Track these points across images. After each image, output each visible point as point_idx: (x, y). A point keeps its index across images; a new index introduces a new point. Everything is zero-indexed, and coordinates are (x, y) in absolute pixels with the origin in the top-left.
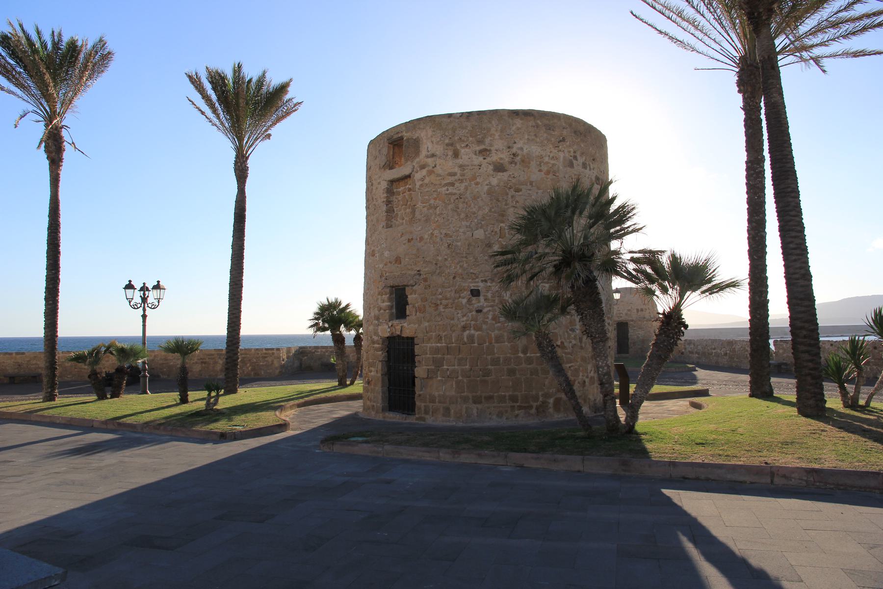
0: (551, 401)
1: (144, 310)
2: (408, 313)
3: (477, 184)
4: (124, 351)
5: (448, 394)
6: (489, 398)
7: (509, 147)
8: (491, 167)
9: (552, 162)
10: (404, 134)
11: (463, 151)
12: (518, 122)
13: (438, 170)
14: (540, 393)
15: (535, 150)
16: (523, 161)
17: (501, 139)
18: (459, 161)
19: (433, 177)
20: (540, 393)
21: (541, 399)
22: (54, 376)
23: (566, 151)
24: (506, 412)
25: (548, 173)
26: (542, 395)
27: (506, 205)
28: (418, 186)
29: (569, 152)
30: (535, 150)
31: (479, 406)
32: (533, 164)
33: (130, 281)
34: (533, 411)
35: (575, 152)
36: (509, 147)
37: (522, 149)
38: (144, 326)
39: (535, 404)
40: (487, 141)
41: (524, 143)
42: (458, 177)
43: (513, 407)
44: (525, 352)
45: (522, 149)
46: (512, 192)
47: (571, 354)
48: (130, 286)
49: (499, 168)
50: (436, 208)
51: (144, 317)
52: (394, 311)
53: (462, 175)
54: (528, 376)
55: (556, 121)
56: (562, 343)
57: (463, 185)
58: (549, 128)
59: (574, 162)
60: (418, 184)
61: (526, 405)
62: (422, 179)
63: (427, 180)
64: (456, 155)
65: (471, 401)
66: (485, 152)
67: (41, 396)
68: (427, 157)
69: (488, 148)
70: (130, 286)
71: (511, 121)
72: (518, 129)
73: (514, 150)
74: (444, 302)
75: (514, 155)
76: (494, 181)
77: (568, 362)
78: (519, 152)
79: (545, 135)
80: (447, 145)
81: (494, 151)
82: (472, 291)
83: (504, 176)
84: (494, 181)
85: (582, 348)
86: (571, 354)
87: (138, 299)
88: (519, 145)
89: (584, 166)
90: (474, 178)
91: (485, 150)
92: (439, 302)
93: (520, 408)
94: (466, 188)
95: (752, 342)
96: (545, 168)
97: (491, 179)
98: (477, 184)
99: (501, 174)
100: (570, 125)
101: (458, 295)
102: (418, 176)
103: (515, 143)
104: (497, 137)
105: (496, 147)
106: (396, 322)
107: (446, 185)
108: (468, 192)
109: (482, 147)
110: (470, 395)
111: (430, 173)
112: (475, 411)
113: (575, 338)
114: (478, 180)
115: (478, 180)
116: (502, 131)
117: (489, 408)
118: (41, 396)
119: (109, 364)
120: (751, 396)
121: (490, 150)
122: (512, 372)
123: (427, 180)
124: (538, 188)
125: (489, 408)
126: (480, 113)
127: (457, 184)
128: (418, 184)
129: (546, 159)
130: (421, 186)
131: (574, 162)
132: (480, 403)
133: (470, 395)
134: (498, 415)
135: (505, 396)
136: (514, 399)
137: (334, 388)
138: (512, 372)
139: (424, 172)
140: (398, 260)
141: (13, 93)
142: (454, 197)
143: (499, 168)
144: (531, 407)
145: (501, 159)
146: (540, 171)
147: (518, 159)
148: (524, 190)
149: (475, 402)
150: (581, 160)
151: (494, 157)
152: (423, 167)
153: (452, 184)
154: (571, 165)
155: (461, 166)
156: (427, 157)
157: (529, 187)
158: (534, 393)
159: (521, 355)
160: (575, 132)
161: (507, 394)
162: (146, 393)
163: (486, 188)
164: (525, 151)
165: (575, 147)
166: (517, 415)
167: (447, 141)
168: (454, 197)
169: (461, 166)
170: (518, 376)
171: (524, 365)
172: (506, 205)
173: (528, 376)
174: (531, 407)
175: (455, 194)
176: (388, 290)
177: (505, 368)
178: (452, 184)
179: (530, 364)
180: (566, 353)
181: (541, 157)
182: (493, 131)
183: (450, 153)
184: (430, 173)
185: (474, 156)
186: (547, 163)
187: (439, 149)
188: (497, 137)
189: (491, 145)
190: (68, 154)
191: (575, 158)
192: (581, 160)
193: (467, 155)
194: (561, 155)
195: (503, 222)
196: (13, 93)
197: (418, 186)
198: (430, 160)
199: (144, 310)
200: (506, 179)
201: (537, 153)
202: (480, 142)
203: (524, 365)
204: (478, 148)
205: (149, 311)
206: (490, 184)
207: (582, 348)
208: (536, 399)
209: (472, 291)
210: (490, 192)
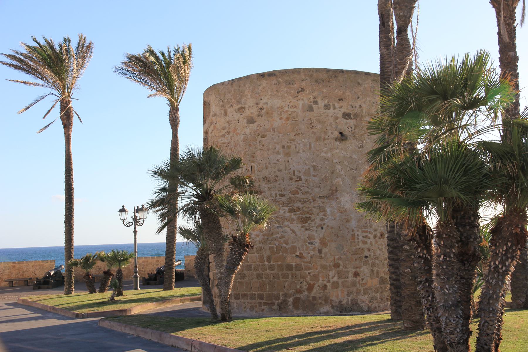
0: (291, 300)
1: (135, 228)
3: (237, 134)
4: (117, 257)
6: (245, 295)
8: (245, 121)
11: (229, 110)
14: (281, 293)
15: (277, 102)
16: (267, 113)
17: (252, 97)
18: (227, 118)
20: (281, 293)
21: (281, 298)
22: (71, 276)
23: (305, 99)
24: (256, 306)
25: (288, 119)
26: (283, 295)
27: (255, 148)
29: (309, 99)
30: (277, 102)
31: (238, 301)
32: (275, 114)
33: (123, 206)
34: (275, 307)
35: (315, 98)
36: (257, 104)
37: (266, 103)
38: (135, 239)
39: (277, 302)
40: (243, 101)
41: (268, 99)
42: (227, 130)
43: (260, 303)
44: (269, 260)
45: (266, 103)
46: (259, 138)
47: (310, 262)
48: (123, 210)
49: (251, 121)
51: (135, 232)
54: (271, 279)
55: (295, 76)
56: (300, 253)
57: (229, 136)
58: (289, 83)
59: (314, 106)
61: (270, 302)
64: (226, 114)
66: (241, 110)
67: (63, 293)
70: (123, 210)
71: (259, 83)
72: (264, 88)
73: (260, 106)
76: (248, 131)
77: (306, 269)
78: (265, 106)
79: (286, 89)
81: (247, 108)
83: (254, 126)
84: (248, 131)
85: (321, 258)
86: (310, 262)
87: (130, 219)
90: (235, 130)
91: (242, 108)
93: (265, 304)
95: (197, 263)
96: (285, 116)
99: (252, 125)
100: (311, 76)
103: (261, 99)
104: (249, 97)
105: (249, 104)
108: (232, 141)
109: (240, 106)
113: (314, 250)
114: (238, 131)
115: (238, 131)
116: (252, 92)
117: (244, 303)
118: (63, 293)
119: (101, 267)
120: (90, 293)
121: (244, 108)
122: (259, 276)
124: (280, 133)
125: (244, 303)
127: (227, 136)
129: (286, 108)
131: (314, 106)
132: (239, 299)
134: (250, 309)
135: (255, 294)
136: (261, 297)
138: (259, 276)
141: (36, 84)
142: (225, 145)
143: (251, 121)
144: (273, 304)
145: (252, 113)
146: (281, 119)
147: (264, 112)
148: (268, 136)
149: (235, 298)
150: (321, 103)
151: (247, 113)
154: (311, 109)
155: (228, 122)
157: (272, 132)
158: (276, 293)
159: (266, 263)
160: (316, 81)
161: (256, 293)
162: (137, 289)
163: (242, 137)
164: (269, 105)
165: (315, 94)
166: (263, 310)
169: (228, 122)
170: (264, 279)
171: (268, 271)
172: (255, 148)
173: (271, 279)
174: (273, 304)
177: (255, 273)
178: (224, 136)
179: (272, 270)
180: (304, 262)
181: (282, 107)
182: (246, 93)
183: (223, 112)
185: (235, 114)
186: (287, 111)
188: (249, 97)
189: (245, 104)
190: (75, 120)
191: (316, 102)
192: (321, 103)
193: (233, 114)
194: (300, 103)
195: (253, 162)
196: (36, 84)
199: (135, 228)
200: (255, 128)
201: (278, 105)
202: (239, 102)
203: (268, 271)
204: (237, 107)
205: (138, 228)
206: (245, 134)
207: (321, 258)
208: (277, 298)
210: (245, 140)
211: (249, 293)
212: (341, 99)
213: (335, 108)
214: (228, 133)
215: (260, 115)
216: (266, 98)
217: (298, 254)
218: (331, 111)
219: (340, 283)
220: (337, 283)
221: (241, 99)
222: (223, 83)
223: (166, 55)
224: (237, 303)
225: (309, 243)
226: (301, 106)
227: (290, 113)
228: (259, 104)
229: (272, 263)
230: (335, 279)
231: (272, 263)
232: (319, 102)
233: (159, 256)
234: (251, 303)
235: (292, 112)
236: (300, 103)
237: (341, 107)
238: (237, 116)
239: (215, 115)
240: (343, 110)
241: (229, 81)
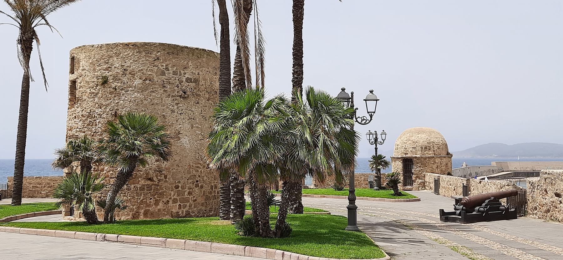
12: (129, 52)
29: (163, 66)
35: (166, 66)
62: (80, 83)
191: (167, 69)
198: (83, 73)
213: (180, 75)
215: (124, 74)
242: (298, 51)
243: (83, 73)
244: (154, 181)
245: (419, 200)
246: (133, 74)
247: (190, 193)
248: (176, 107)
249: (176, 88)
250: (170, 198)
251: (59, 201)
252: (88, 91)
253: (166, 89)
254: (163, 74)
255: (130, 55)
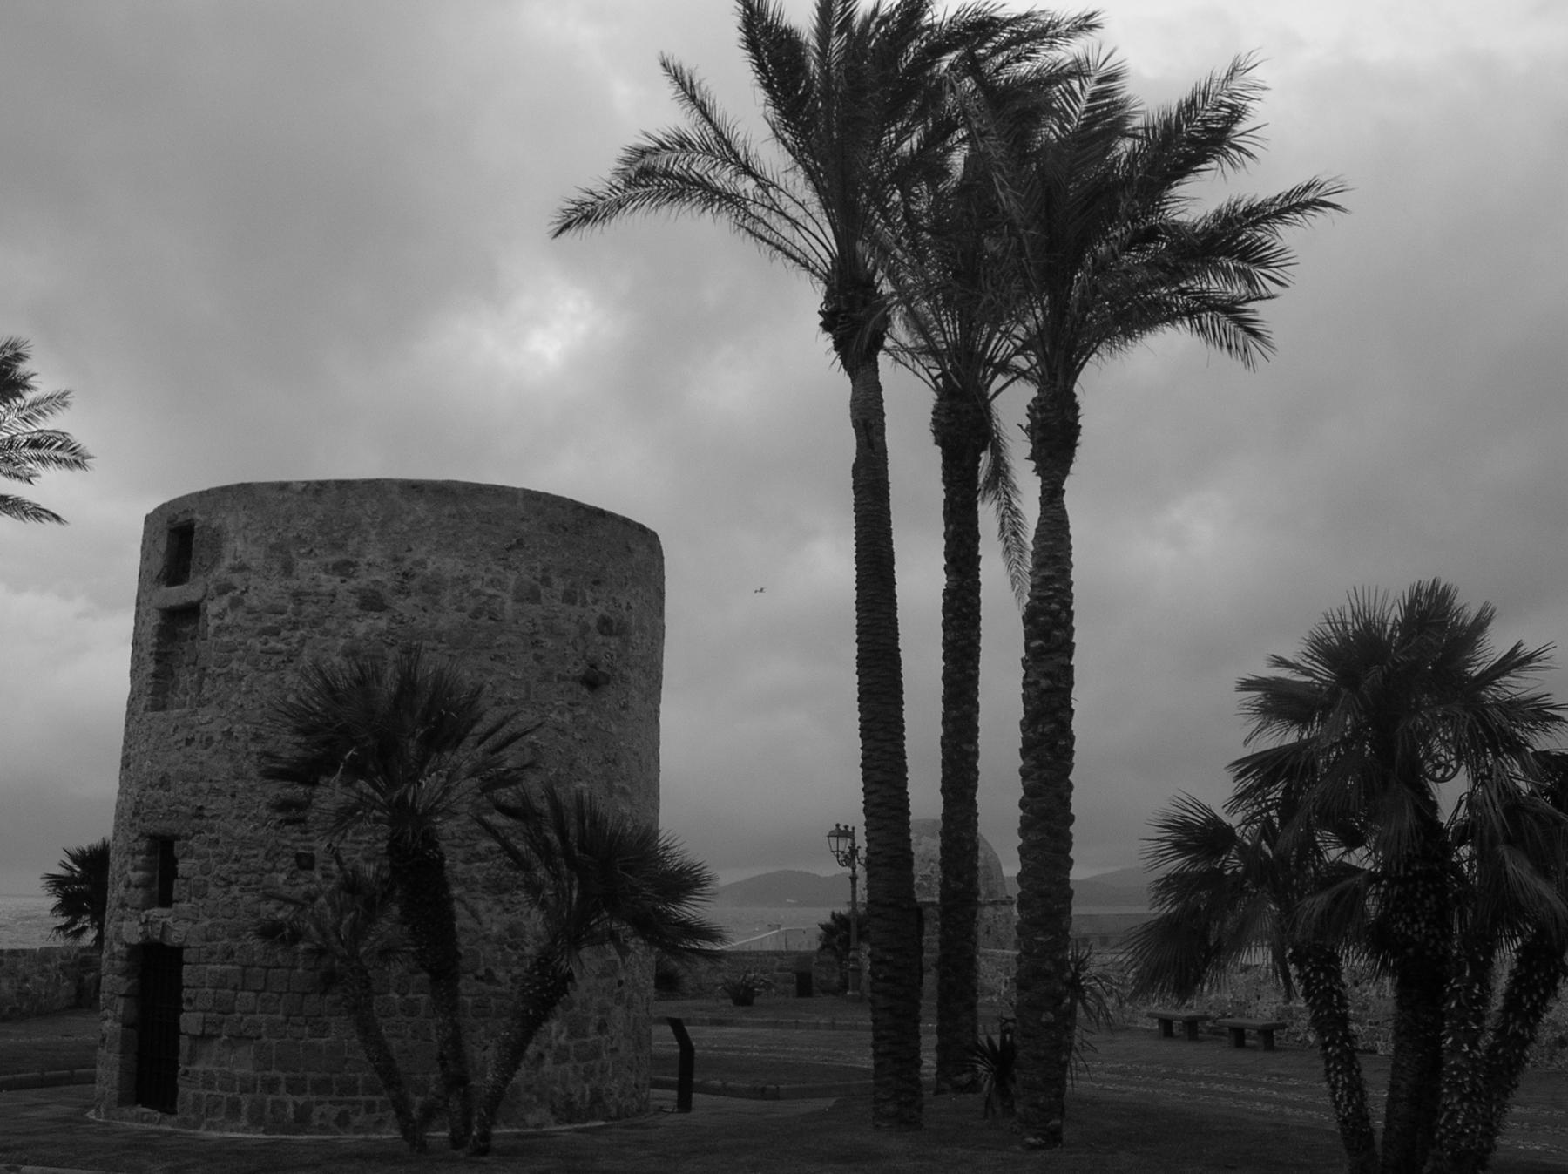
2: (175, 895)
5: (237, 1071)
7: (396, 560)
8: (355, 599)
9: (490, 591)
10: (197, 516)
12: (421, 508)
13: (252, 600)
16: (424, 588)
19: (240, 612)
25: (476, 614)
28: (211, 630)
29: (533, 569)
30: (450, 565)
31: (301, 1100)
35: (545, 570)
37: (422, 563)
40: (353, 544)
42: (289, 615)
45: (422, 563)
49: (372, 602)
50: (240, 679)
52: (156, 889)
53: (298, 613)
56: (488, 972)
60: (213, 623)
62: (220, 616)
63: (228, 620)
64: (288, 569)
65: (282, 1088)
66: (344, 569)
68: (234, 570)
69: (353, 560)
73: (407, 565)
74: (243, 879)
75: (405, 575)
76: (361, 629)
78: (417, 570)
80: (272, 547)
81: (363, 566)
82: (298, 857)
88: (419, 553)
89: (569, 598)
91: (348, 564)
92: (233, 878)
94: (302, 641)
96: (471, 604)
97: (354, 623)
98: (326, 633)
101: (269, 865)
102: (213, 608)
103: (410, 550)
104: (373, 536)
106: (156, 912)
107: (264, 632)
109: (339, 557)
110: (282, 1076)
111: (236, 603)
112: (290, 1109)
117: (319, 1103)
121: (354, 565)
123: (228, 620)
126: (343, 485)
127: (284, 633)
128: (213, 623)
129: (477, 585)
130: (219, 629)
133: (282, 1076)
137: (1010, 515)
139: (225, 600)
140: (164, 783)
143: (372, 602)
146: (460, 610)
151: (363, 580)
152: (224, 589)
153: (275, 632)
156: (234, 570)
160: (551, 527)
164: (430, 567)
167: (272, 540)
168: (277, 659)
175: (279, 653)
176: (143, 844)
178: (275, 632)
181: (465, 580)
183: (277, 566)
184: (236, 603)
185: (323, 576)
187: (255, 556)
188: (373, 536)
191: (546, 581)
192: (559, 585)
193: (311, 572)
197: (211, 630)
198: (236, 579)
202: (337, 546)
204: (332, 559)
209: (298, 857)
211: (336, 1076)
212: (597, 583)
213: (584, 604)
214: (295, 626)
215: (402, 590)
216: (424, 549)
217: (481, 972)
218: (575, 610)
219: (572, 1049)
220: (567, 1049)
221: (345, 538)
222: (283, 486)
223: (1380, 597)
224: (295, 1104)
225: (510, 946)
226: (512, 584)
227: (484, 599)
228: (403, 560)
229: (410, 996)
230: (562, 1039)
231: (410, 996)
232: (555, 581)
233: (843, 833)
234: (341, 1103)
235: (491, 596)
236: (512, 579)
237: (595, 602)
238: (329, 582)
239: (241, 568)
240: (600, 610)
241: (308, 483)
242: (871, 444)
243: (236, 579)
244: (499, 983)
245: (1344, 210)
246: (432, 589)
247: (602, 1027)
248: (568, 717)
249: (570, 650)
250: (549, 1046)
251: (919, 870)
252: (256, 644)
253: (540, 652)
254: (534, 597)
255: (428, 523)
